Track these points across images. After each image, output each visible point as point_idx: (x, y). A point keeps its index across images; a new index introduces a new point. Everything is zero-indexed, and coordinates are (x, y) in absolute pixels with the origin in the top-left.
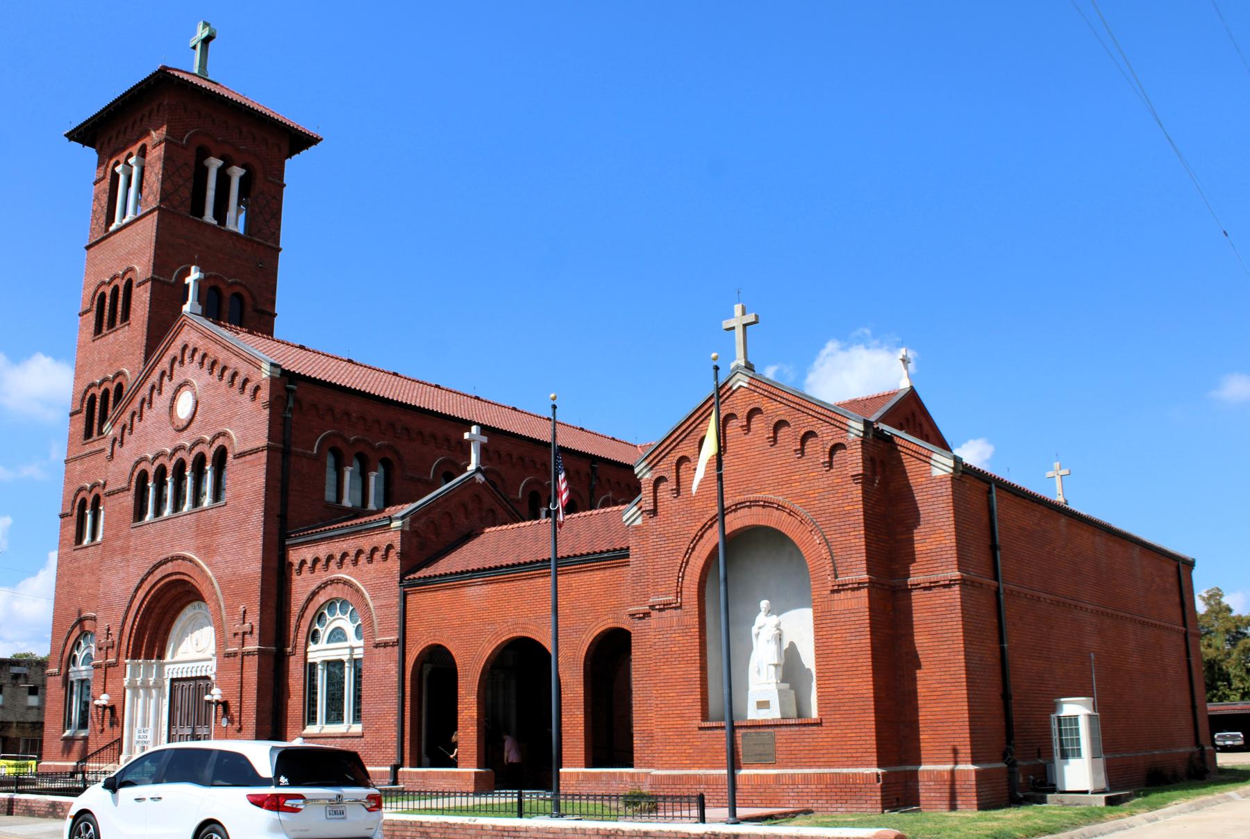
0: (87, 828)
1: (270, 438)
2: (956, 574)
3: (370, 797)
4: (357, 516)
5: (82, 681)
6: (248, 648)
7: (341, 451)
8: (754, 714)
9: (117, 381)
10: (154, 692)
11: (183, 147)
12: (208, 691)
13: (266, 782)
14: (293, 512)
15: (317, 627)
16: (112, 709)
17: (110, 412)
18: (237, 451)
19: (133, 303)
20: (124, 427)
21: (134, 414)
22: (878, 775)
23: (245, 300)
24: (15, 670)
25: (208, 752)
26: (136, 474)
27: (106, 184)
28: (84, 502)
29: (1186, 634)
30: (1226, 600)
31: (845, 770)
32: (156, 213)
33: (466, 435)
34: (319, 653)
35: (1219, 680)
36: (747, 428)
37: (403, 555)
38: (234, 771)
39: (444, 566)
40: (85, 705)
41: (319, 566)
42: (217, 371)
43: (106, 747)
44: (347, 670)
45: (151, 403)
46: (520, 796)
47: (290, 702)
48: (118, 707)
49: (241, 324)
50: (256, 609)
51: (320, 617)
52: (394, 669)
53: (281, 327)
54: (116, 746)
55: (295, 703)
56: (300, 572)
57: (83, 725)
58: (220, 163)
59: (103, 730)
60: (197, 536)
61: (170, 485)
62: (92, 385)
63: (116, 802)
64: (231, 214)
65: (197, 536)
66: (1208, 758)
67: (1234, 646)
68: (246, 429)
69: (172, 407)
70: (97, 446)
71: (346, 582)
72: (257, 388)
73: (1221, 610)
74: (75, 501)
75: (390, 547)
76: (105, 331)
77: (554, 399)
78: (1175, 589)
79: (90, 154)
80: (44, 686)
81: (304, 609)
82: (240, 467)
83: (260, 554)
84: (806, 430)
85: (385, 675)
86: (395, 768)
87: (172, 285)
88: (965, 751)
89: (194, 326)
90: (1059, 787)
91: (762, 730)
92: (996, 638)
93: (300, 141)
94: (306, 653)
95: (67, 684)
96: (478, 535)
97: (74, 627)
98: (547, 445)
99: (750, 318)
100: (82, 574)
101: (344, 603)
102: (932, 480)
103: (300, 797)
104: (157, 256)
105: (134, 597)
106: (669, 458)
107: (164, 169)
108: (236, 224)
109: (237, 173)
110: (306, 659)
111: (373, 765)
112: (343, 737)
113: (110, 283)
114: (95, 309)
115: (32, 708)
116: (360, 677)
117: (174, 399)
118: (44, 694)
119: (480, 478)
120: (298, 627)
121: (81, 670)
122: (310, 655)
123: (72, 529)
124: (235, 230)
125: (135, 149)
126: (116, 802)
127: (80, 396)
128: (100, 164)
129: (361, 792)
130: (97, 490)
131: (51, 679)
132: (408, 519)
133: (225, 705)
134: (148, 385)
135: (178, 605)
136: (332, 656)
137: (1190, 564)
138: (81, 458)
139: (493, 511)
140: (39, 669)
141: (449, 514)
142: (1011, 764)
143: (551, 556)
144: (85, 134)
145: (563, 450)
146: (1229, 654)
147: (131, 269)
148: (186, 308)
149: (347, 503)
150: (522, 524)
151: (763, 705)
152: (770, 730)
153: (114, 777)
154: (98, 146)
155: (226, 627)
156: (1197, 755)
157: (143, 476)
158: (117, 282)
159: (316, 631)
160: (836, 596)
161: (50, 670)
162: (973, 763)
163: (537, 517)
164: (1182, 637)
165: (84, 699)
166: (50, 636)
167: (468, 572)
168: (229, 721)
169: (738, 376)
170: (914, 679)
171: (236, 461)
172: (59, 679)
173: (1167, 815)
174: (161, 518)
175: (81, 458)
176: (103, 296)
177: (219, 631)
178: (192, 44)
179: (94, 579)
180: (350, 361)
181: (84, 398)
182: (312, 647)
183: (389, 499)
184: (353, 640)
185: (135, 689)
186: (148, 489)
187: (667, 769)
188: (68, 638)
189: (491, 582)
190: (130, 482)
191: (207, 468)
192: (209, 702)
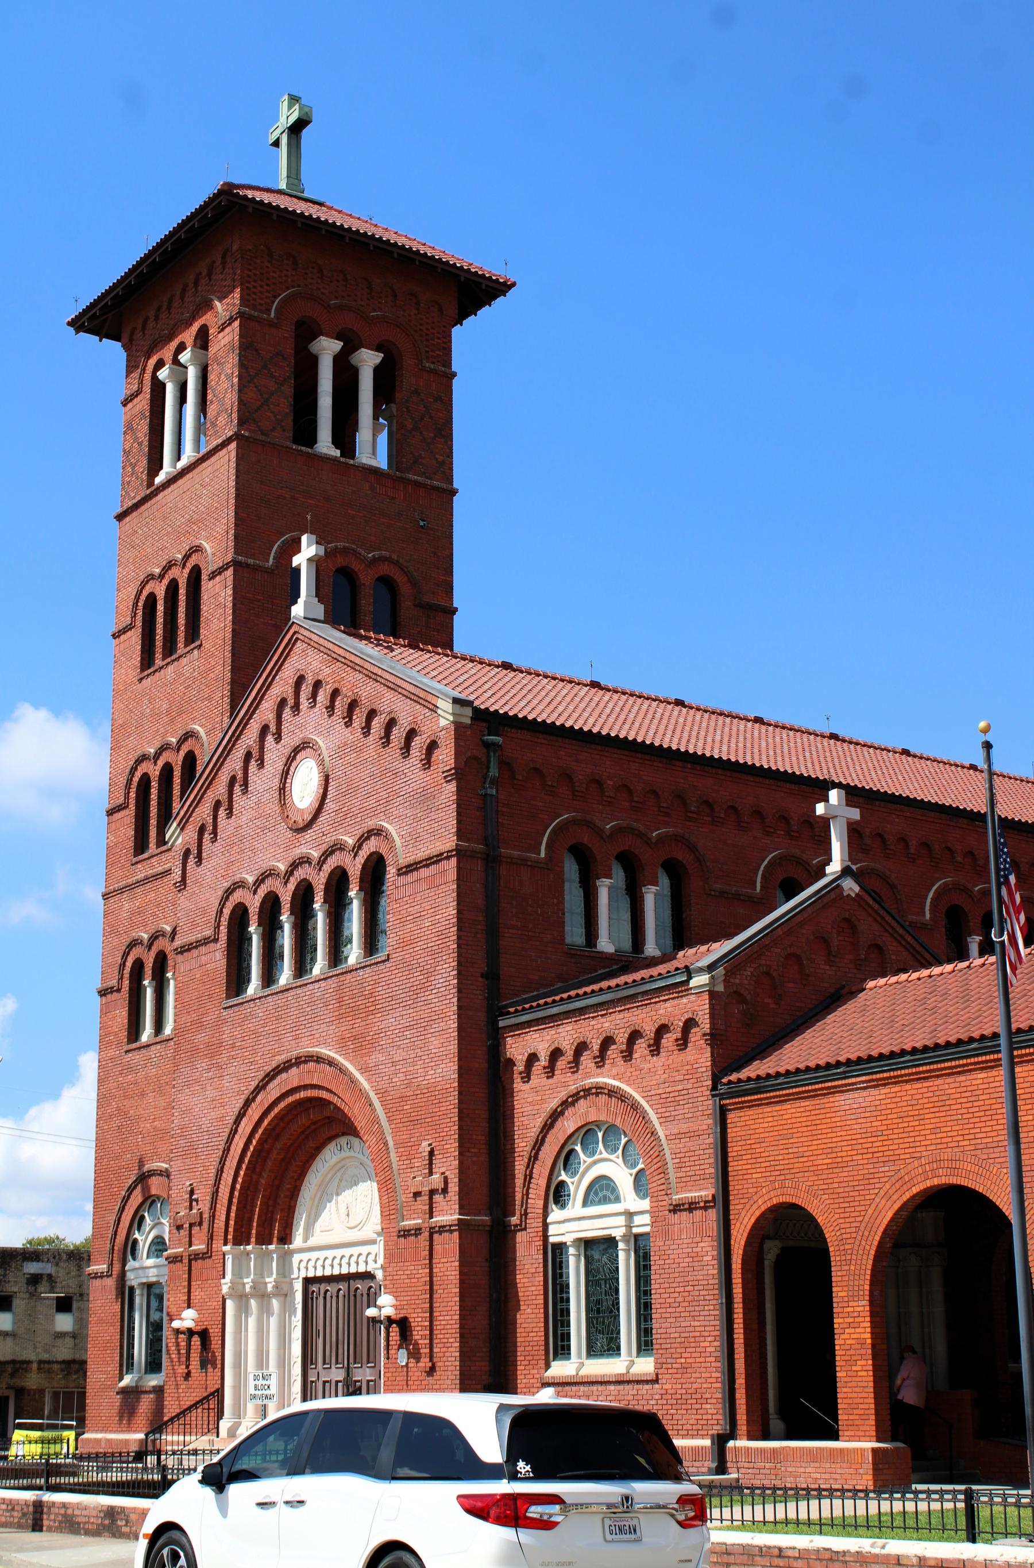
0: (175, 1557)
1: (460, 834)
3: (684, 1500)
4: (625, 969)
5: (149, 1286)
6: (439, 1219)
7: (597, 850)
9: (185, 749)
10: (275, 1303)
11: (272, 324)
12: (371, 1302)
13: (491, 1472)
14: (513, 968)
15: (564, 1177)
16: (204, 1335)
17: (176, 805)
18: (403, 862)
19: (204, 608)
20: (202, 830)
21: (217, 805)
23: (400, 591)
24: (32, 1268)
25: (384, 1416)
26: (227, 912)
27: (143, 402)
28: (138, 966)
32: (233, 446)
33: (820, 809)
34: (570, 1224)
37: (714, 1038)
38: (434, 1451)
39: (791, 1056)
40: (155, 1329)
41: (561, 1064)
42: (359, 719)
43: (195, 1405)
44: (622, 1255)
45: (245, 784)
46: (969, 1496)
47: (520, 1318)
48: (214, 1332)
49: (394, 632)
50: (452, 1146)
51: (567, 1158)
52: (709, 1251)
53: (465, 633)
54: (213, 1403)
55: (530, 1320)
56: (527, 1076)
57: (154, 1365)
58: (337, 345)
59: (188, 1375)
60: (340, 1017)
61: (287, 928)
62: (143, 758)
63: (223, 1510)
64: (364, 435)
65: (340, 1017)
68: (416, 819)
69: (283, 790)
70: (157, 866)
71: (612, 1093)
72: (432, 746)
74: (123, 965)
75: (690, 1024)
76: (159, 662)
77: (985, 731)
79: (113, 351)
80: (83, 1296)
81: (539, 1144)
82: (410, 890)
83: (453, 1047)
85: (693, 1261)
86: (721, 1441)
87: (269, 572)
89: (315, 643)
93: (476, 291)
94: (545, 1226)
95: (125, 1293)
96: (853, 994)
97: (131, 1189)
98: (976, 818)
100: (143, 1095)
101: (611, 1131)
103: (553, 1499)
104: (240, 522)
105: (233, 1132)
107: (242, 365)
108: (374, 453)
109: (368, 360)
110: (545, 1237)
111: (683, 1437)
112: (620, 1381)
113: (162, 576)
114: (139, 623)
115: (61, 1335)
116: (647, 1267)
117: (286, 774)
118: (84, 1311)
119: (850, 886)
120: (529, 1177)
121: (145, 1267)
122: (552, 1230)
123: (121, 1014)
124: (373, 463)
125: (188, 336)
126: (223, 1510)
127: (123, 780)
128: (130, 369)
129: (665, 1490)
130: (161, 944)
131: (97, 1283)
132: (720, 971)
133: (403, 1324)
134: (239, 753)
135: (311, 1144)
136: (593, 1230)
138: (130, 887)
139: (878, 948)
140: (72, 1266)
141: (798, 957)
143: (1000, 1028)
144: (102, 318)
145: (1008, 825)
147: (197, 549)
148: (297, 610)
149: (605, 945)
150: (936, 970)
153: (219, 1463)
154: (125, 336)
155: (398, 1182)
157: (240, 914)
158: (174, 572)
159: (562, 1184)
161: (94, 1268)
163: (962, 954)
165: (155, 1316)
166: (89, 1207)
167: (838, 1064)
168: (410, 1355)
171: (403, 880)
172: (110, 1283)
174: (274, 988)
175: (130, 887)
176: (152, 599)
177: (387, 1189)
178: (272, 138)
179: (162, 1103)
180: (595, 685)
181: (129, 782)
182: (556, 1214)
183: (682, 936)
184: (631, 1200)
185: (242, 1299)
186: (255, 933)
188: (122, 1210)
189: (885, 1083)
190: (218, 927)
191: (352, 894)
192: (374, 1320)
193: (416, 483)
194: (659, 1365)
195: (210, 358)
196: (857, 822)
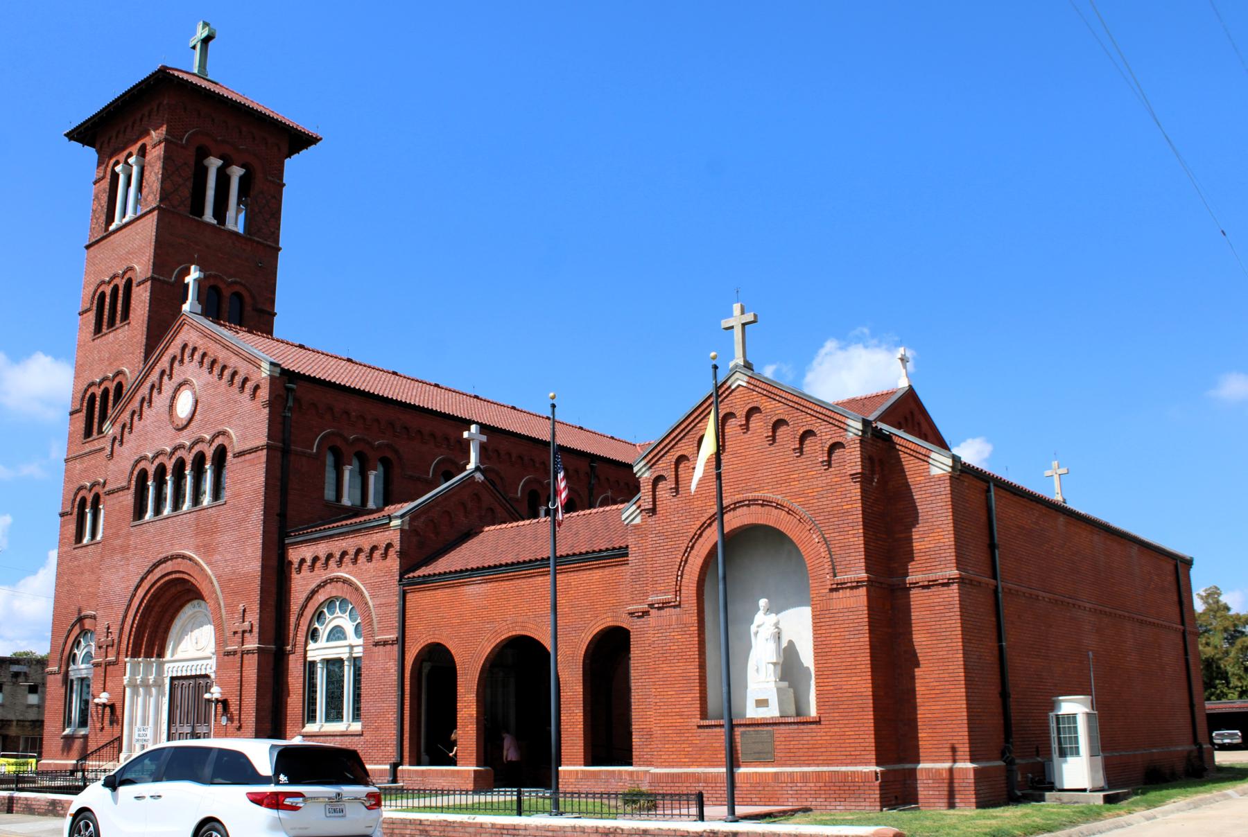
0: (87, 826)
1: (269, 437)
2: (954, 573)
3: (369, 795)
4: (356, 515)
5: (82, 680)
6: (247, 646)
7: (340, 450)
8: (752, 712)
9: (117, 380)
10: (154, 690)
11: (183, 147)
12: (208, 689)
13: (265, 780)
14: (293, 511)
15: (317, 625)
16: (112, 707)
17: (110, 411)
18: (237, 450)
19: (133, 302)
20: (124, 426)
21: (134, 413)
22: (876, 773)
23: (245, 299)
24: (15, 668)
25: (208, 750)
26: (136, 473)
27: (105, 184)
28: (83, 500)
29: (1184, 633)
30: (1224, 599)
31: (844, 769)
32: (156, 213)
33: (466, 434)
34: (319, 651)
35: (1217, 678)
36: (746, 427)
37: (402, 554)
38: (234, 769)
39: (443, 565)
40: (85, 703)
41: (318, 564)
42: (216, 370)
43: (106, 745)
44: (346, 668)
45: (150, 402)
46: (519, 794)
47: (290, 700)
48: (118, 705)
49: (241, 324)
50: (256, 607)
51: (319, 616)
52: (393, 667)
53: (280, 326)
54: (116, 744)
55: (295, 702)
56: (299, 570)
57: (83, 723)
58: (219, 162)
59: (102, 729)
60: (197, 534)
61: (170, 484)
62: (92, 384)
63: (115, 800)
64: (231, 213)
65: (197, 534)
66: (1206, 756)
67: (1232, 644)
68: (246, 428)
69: (172, 407)
70: (97, 445)
71: (345, 581)
72: (257, 387)
73: (1219, 609)
74: (74, 500)
75: (389, 546)
76: (104, 330)
77: (553, 398)
78: (1173, 588)
79: (90, 153)
80: (44, 684)
81: (304, 607)
82: (239, 466)
83: (259, 553)
84: (805, 429)
85: (385, 673)
86: (395, 766)
87: (171, 285)
88: (964, 749)
89: (194, 326)
90: (1058, 785)
91: (760, 728)
92: (994, 636)
93: (300, 141)
94: (306, 652)
95: (67, 682)
96: (477, 534)
97: (73, 625)
98: (546, 444)
99: (749, 317)
100: (82, 573)
101: (344, 602)
102: (930, 478)
103: (299, 795)
104: (156, 255)
105: (134, 595)
106: (668, 457)
107: (164, 168)
108: (236, 223)
109: (236, 172)
110: (305, 657)
111: (372, 763)
112: (343, 735)
113: (109, 282)
114: (95, 308)
115: (32, 706)
116: (360, 675)
117: (173, 398)
118: (44, 693)
119: (479, 477)
120: (297, 625)
121: (81, 669)
122: (309, 654)
123: (72, 528)
124: (235, 229)
125: (135, 149)
126: (115, 800)
127: (80, 395)
128: (100, 164)
129: (360, 790)
130: (97, 489)
131: (51, 677)
132: (407, 518)
133: (225, 703)
134: (148, 384)
135: (178, 603)
136: (331, 654)
137: (1188, 563)
138: (81, 456)
139: (492, 510)
140: (39, 668)
141: (448, 513)
142: (1010, 763)
143: (551, 554)
144: (85, 134)
145: (562, 449)
146: (1227, 653)
147: (131, 269)
148: (186, 307)
149: (346, 501)
150: (521, 523)
151: (762, 703)
152: (769, 728)
153: (114, 775)
154: (98, 146)
155: (226, 625)
156: (1195, 754)
157: (143, 475)
158: (117, 281)
159: (316, 629)
160: (835, 594)
161: (50, 669)
162: (972, 761)
163: (536, 516)
164: (1180, 635)
165: (84, 697)
166: (49, 634)
167: (467, 570)
168: (228, 719)
169: (737, 375)
170: (913, 678)
171: (235, 460)
172: (59, 677)
173: (1166, 813)
174: (160, 517)
175: (81, 456)
176: (103, 295)
177: (219, 629)
178: (192, 44)
179: (94, 577)
180: (349, 360)
181: (84, 397)
182: (311, 645)
183: (389, 498)
184: (352, 639)
185: (135, 687)
186: (147, 487)
187: (666, 767)
188: (68, 637)
189: (491, 581)
190: (130, 481)
191: (207, 466)
192: (209, 701)
195: (145, 165)
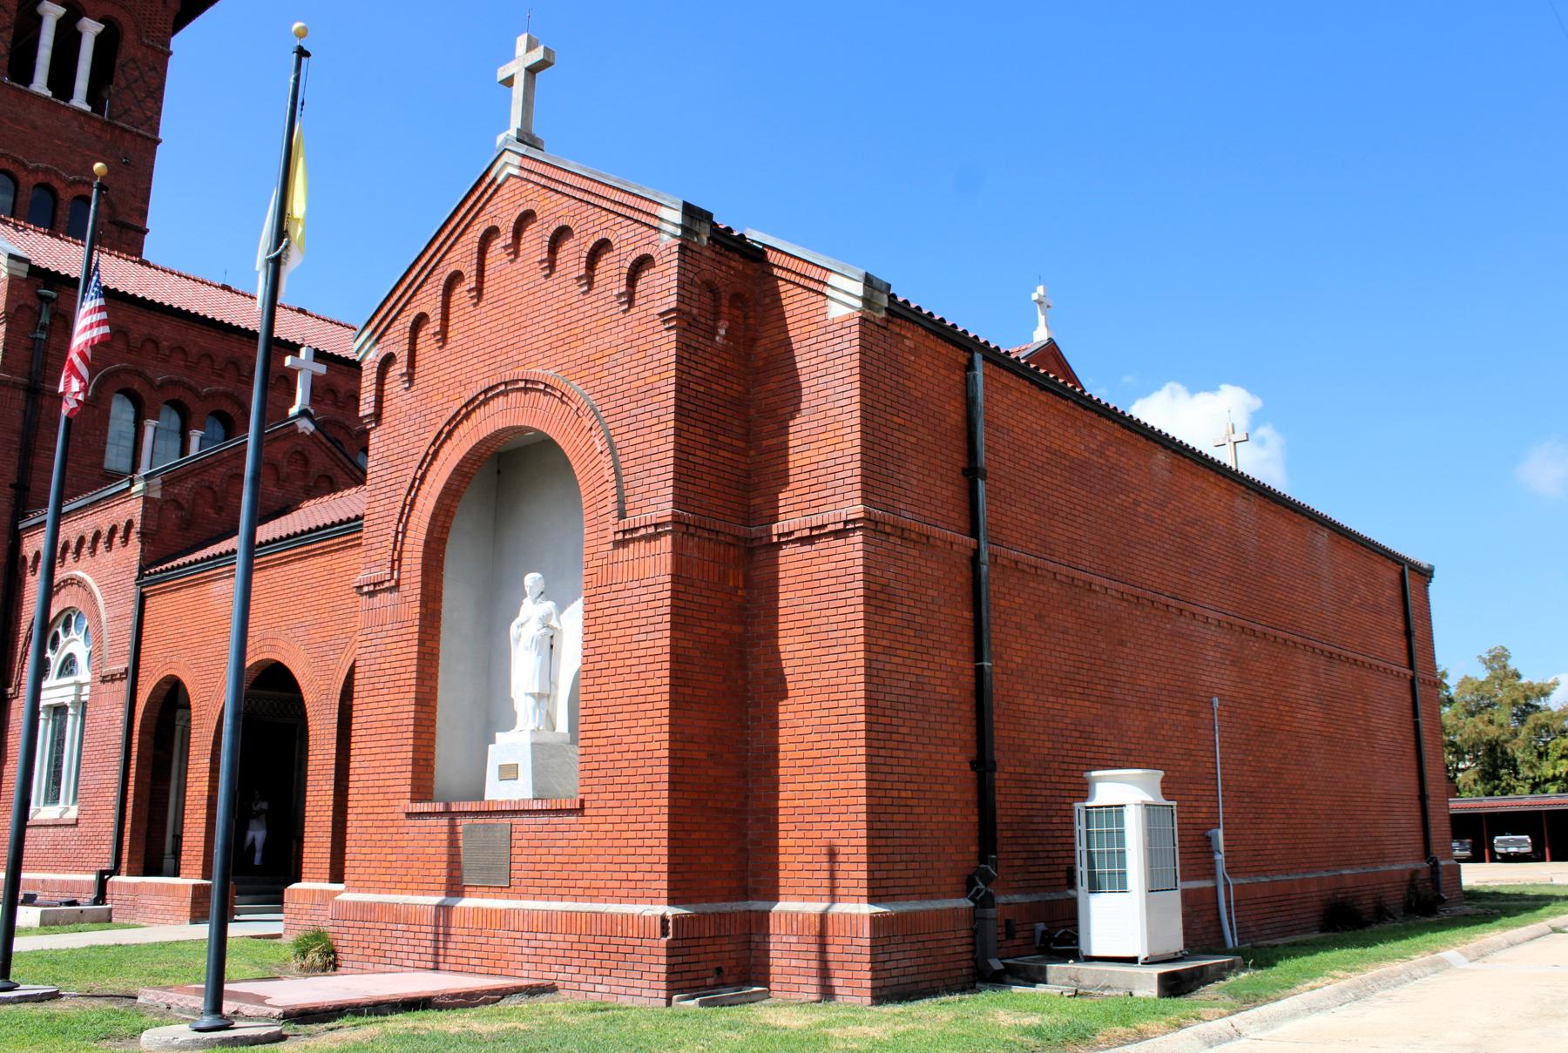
8: (498, 792)
22: (664, 920)
29: (1413, 680)
30: (1513, 664)
35: (1502, 767)
37: (143, 535)
44: (70, 719)
66: (1444, 879)
67: (1522, 722)
73: (1506, 676)
78: (1397, 608)
84: (596, 238)
86: (103, 877)
88: (855, 871)
90: (1083, 947)
91: (493, 820)
92: (967, 645)
99: (537, 55)
102: (827, 327)
109: (90, 29)
119: (306, 426)
137: (1426, 574)
142: (984, 902)
146: (1515, 734)
151: (508, 772)
152: (506, 821)
156: (1424, 875)
160: (622, 553)
162: (873, 899)
164: (1407, 685)
169: (507, 157)
170: (775, 726)
173: (1266, 1024)
193: (123, 129)
194: (81, 811)
196: (20, 279)
